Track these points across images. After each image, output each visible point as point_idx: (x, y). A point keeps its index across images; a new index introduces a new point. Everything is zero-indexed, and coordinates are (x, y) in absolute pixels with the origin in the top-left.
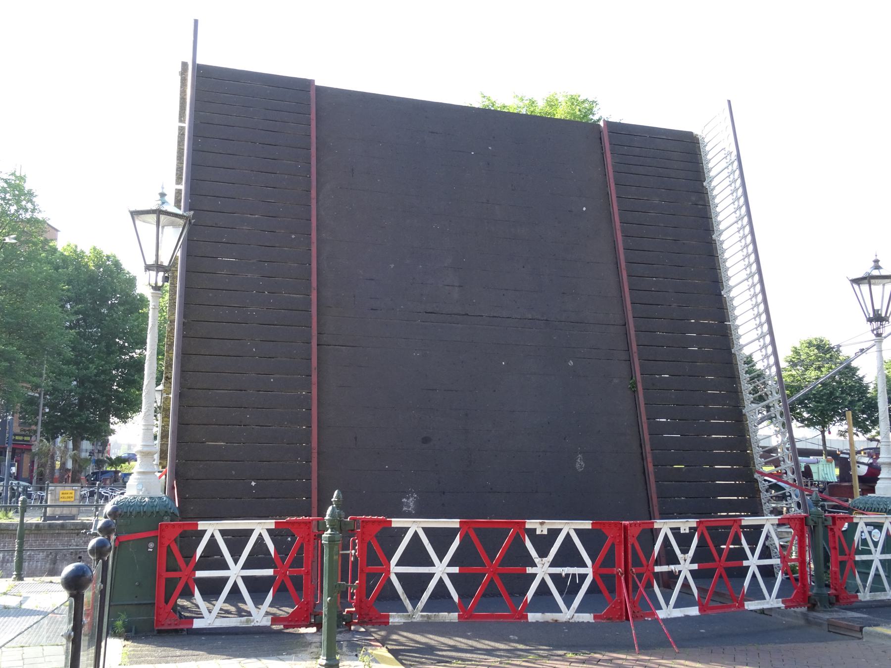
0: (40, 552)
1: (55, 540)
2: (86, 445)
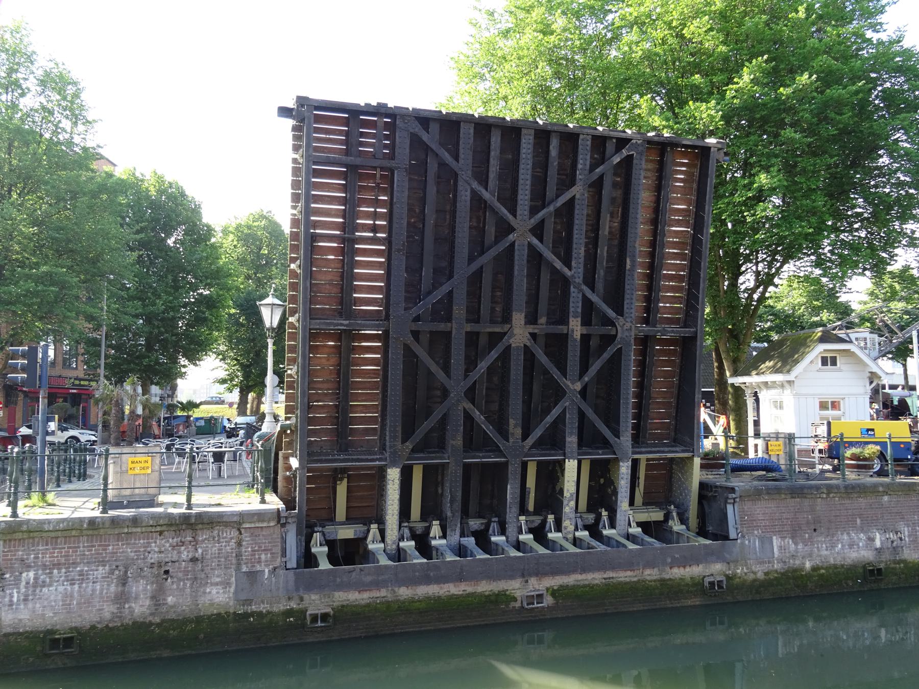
0: (98, 566)
1: (123, 545)
2: (155, 389)
